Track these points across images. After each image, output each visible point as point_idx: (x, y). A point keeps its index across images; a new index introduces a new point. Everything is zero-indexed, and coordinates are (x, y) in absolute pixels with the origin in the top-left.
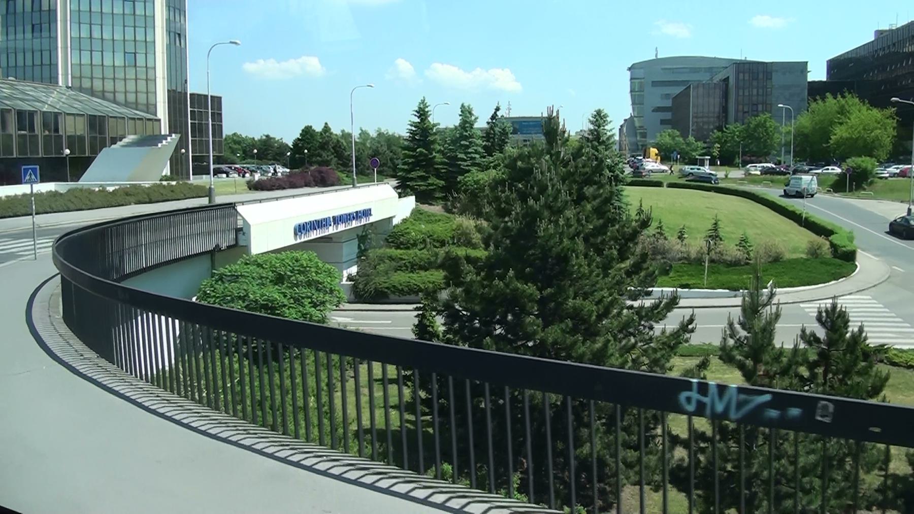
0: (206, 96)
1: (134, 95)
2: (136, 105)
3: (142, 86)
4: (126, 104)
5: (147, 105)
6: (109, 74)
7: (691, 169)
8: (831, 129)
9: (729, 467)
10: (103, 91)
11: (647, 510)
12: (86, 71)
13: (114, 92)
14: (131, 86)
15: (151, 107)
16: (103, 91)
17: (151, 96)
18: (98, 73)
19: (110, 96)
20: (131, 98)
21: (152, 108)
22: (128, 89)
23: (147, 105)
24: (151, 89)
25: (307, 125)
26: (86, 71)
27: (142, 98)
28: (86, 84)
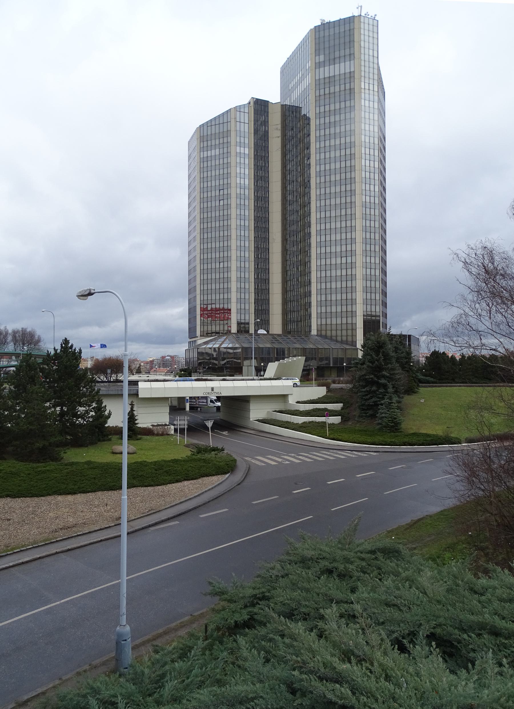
0: (406, 335)
1: (346, 337)
2: (347, 343)
3: (350, 332)
4: (342, 342)
5: (352, 341)
6: (334, 327)
7: (148, 377)
8: (417, 390)
9: (23, 416)
10: (331, 336)
11: (1, 572)
12: (324, 327)
13: (336, 336)
14: (344, 333)
15: (354, 343)
16: (331, 336)
17: (354, 337)
18: (329, 328)
19: (334, 338)
20: (344, 338)
21: (354, 344)
22: (348, 334)
23: (352, 341)
24: (354, 334)
25: (39, 332)
26: (324, 327)
27: (350, 339)
28: (323, 333)
